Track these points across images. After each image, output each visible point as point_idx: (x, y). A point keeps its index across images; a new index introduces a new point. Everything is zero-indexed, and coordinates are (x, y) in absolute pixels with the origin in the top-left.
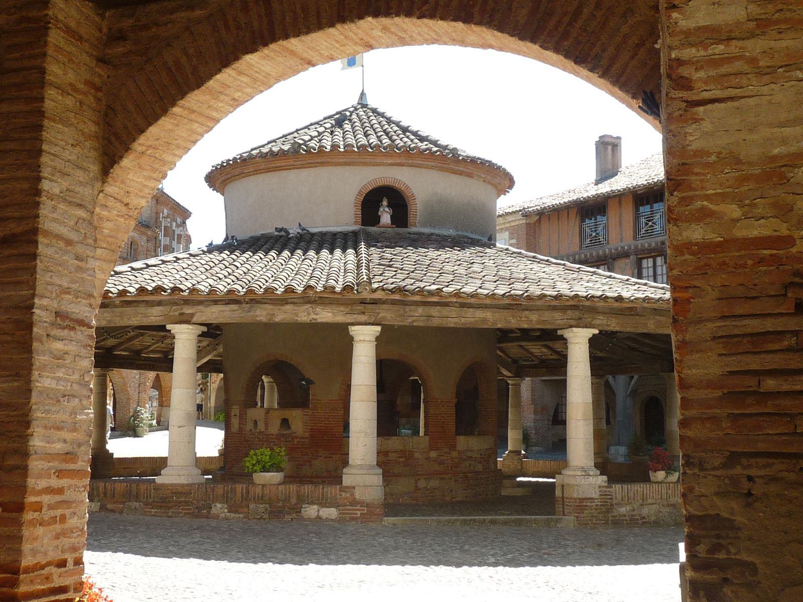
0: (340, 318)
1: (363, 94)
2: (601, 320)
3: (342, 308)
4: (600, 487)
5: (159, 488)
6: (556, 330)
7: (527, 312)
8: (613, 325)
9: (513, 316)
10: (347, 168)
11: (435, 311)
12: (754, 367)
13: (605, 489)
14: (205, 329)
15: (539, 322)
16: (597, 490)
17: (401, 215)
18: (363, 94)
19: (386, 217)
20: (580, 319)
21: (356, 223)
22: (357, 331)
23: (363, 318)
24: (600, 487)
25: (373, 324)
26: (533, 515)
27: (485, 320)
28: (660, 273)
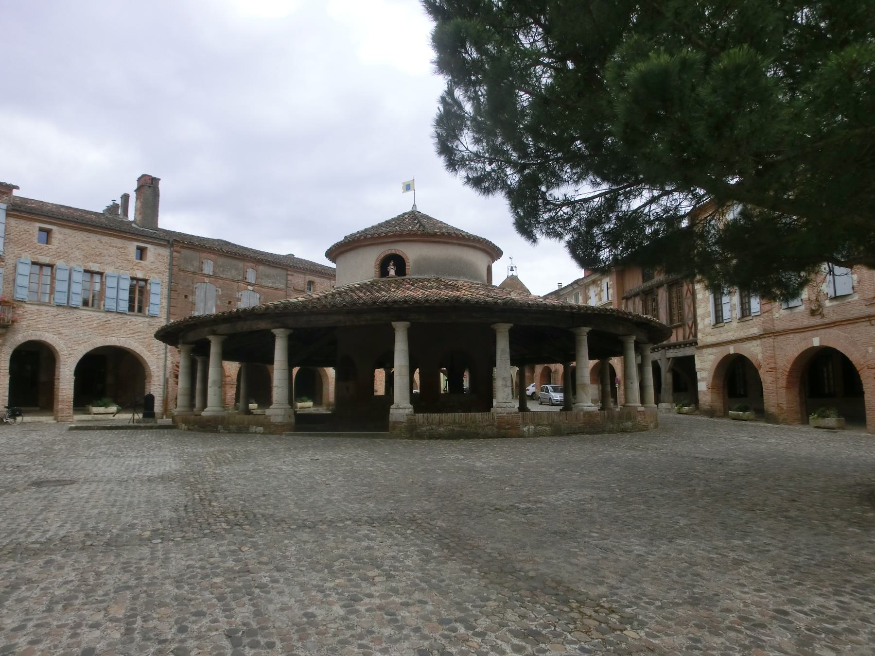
1: (414, 205)
17: (401, 269)
18: (414, 205)
19: (392, 272)
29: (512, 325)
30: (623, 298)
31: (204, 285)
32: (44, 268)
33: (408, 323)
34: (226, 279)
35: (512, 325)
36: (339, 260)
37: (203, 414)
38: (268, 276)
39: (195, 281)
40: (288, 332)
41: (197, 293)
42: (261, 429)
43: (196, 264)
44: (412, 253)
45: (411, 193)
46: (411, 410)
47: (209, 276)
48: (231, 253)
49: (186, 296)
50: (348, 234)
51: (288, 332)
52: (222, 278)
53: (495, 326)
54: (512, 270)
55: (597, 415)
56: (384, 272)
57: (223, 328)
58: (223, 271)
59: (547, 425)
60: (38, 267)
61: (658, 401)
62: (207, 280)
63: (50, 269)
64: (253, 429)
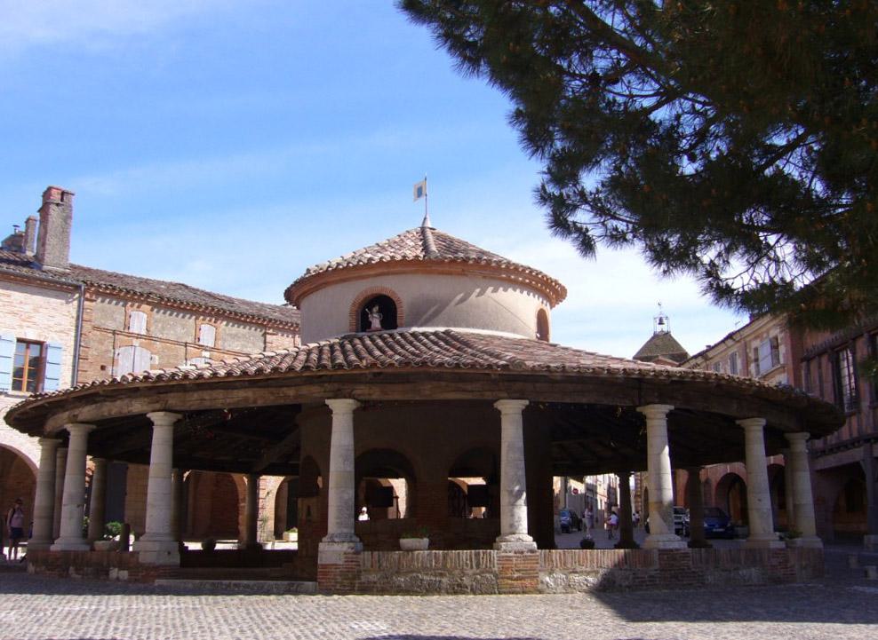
0: (145, 408)
2: (361, 390)
3: (146, 399)
4: (345, 553)
5: (675, 404)
6: (146, 414)
7: (285, 389)
8: (375, 394)
9: (272, 393)
10: (345, 284)
11: (206, 395)
12: (825, 385)
13: (350, 556)
14: (180, 416)
15: (296, 397)
16: (343, 557)
17: (390, 320)
19: (376, 322)
20: (339, 390)
21: (351, 331)
22: (334, 404)
23: (158, 406)
24: (345, 553)
25: (159, 411)
26: (233, 579)
27: (246, 399)
28: (847, 373)
29: (527, 402)
30: (802, 360)
31: (131, 350)
32: (32, 346)
33: (351, 401)
34: (167, 341)
35: (527, 402)
36: (305, 303)
37: (53, 548)
38: (235, 337)
39: (118, 343)
40: (173, 417)
41: (120, 362)
42: (124, 574)
43: (121, 318)
44: (405, 291)
45: (423, 199)
46: (179, 561)
47: (139, 336)
48: (236, 314)
49: (103, 368)
50: (313, 267)
51: (173, 417)
52: (160, 340)
53: (746, 423)
54: (661, 323)
55: (685, 555)
56: (364, 325)
57: (87, 412)
58: (163, 328)
59: (589, 573)
60: (24, 345)
61: (676, 523)
62: (136, 342)
63: (38, 347)
64: (114, 573)
